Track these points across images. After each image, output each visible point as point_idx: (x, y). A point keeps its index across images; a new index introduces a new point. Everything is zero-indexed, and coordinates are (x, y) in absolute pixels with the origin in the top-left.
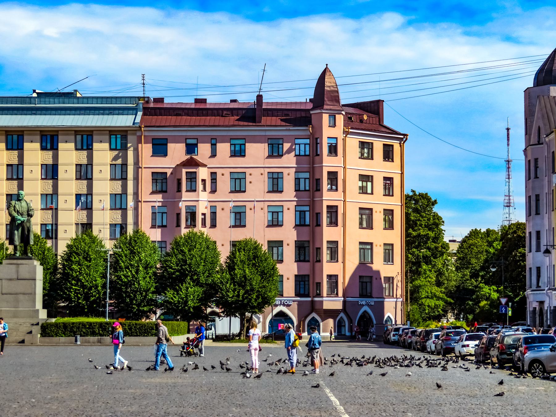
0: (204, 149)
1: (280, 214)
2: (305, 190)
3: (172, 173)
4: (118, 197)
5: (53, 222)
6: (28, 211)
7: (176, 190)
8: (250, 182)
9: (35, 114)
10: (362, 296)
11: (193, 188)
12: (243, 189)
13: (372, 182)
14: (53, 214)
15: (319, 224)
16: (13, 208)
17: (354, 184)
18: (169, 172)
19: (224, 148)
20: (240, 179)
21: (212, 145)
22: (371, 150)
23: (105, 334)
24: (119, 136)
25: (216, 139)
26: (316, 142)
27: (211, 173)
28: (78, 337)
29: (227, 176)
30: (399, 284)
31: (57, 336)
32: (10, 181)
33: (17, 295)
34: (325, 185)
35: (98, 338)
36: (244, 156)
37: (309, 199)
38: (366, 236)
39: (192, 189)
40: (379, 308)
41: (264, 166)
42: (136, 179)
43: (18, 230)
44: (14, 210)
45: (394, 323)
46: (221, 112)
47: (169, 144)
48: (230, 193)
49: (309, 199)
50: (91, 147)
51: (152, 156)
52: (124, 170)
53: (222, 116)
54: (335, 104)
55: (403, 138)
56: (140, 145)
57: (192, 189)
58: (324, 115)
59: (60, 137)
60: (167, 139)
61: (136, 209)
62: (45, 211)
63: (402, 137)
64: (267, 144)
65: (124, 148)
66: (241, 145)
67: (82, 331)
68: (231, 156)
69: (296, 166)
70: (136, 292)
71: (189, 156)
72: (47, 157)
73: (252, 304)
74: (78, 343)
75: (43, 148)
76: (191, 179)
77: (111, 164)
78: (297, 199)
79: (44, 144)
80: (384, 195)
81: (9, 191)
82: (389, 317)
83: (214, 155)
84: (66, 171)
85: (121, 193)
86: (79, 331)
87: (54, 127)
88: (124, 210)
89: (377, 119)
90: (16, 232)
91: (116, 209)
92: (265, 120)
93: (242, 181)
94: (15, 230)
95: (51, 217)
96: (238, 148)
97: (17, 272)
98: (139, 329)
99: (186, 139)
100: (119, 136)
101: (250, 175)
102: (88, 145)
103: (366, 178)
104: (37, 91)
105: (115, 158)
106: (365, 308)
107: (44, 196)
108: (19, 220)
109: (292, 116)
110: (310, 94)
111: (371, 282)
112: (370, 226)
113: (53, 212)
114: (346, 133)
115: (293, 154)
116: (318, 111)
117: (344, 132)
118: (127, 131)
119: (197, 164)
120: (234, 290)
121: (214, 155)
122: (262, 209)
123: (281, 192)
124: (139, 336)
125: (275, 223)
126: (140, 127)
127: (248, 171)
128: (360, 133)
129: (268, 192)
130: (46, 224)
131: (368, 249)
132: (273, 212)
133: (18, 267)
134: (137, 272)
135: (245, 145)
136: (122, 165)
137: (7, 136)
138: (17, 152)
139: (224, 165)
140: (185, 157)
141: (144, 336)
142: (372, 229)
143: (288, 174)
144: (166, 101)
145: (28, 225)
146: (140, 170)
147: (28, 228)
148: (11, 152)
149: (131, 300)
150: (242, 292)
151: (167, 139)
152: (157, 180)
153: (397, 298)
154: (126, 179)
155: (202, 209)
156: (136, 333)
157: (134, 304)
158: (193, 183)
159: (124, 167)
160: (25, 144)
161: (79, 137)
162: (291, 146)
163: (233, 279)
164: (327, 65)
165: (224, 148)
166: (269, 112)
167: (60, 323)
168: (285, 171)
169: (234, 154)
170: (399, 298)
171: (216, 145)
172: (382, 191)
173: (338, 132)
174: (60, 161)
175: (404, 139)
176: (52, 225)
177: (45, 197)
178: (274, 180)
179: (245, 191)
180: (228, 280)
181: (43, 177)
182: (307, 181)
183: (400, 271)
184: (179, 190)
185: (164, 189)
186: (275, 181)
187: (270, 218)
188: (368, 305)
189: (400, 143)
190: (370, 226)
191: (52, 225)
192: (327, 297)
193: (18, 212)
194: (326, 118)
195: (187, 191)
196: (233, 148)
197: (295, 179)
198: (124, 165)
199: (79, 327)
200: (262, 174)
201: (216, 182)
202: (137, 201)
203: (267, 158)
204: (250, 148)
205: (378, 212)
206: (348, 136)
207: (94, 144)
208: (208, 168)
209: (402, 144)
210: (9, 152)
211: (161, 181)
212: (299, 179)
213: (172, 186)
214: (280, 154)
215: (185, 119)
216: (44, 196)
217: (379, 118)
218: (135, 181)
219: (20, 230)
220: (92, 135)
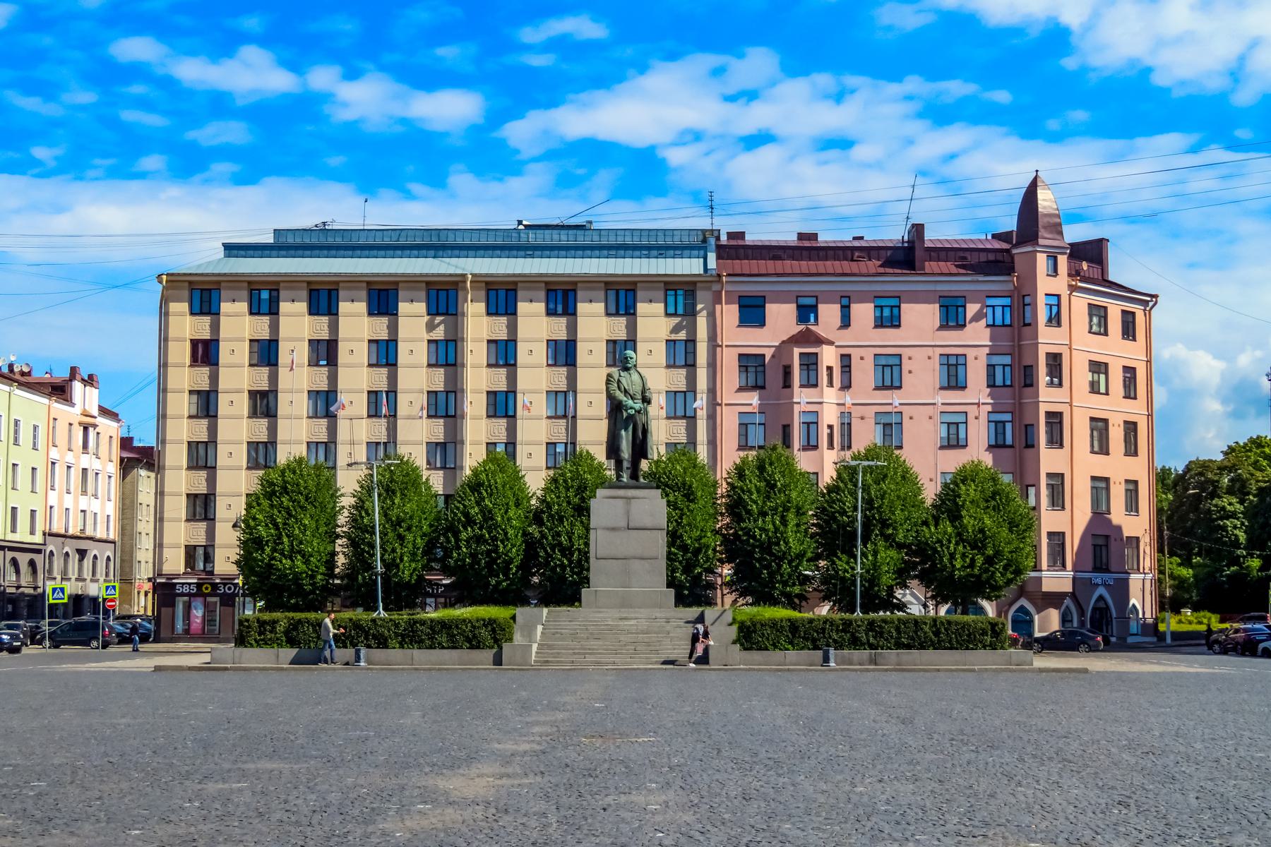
0: (829, 314)
1: (962, 427)
2: (1005, 386)
3: (773, 356)
4: (680, 398)
5: (567, 440)
6: (644, 391)
7: (781, 384)
8: (910, 372)
9: (532, 256)
10: (1097, 569)
11: (813, 381)
12: (896, 384)
13: (1106, 373)
14: (567, 426)
15: (1031, 444)
16: (616, 385)
17: (1080, 375)
18: (768, 353)
19: (863, 312)
20: (891, 366)
21: (842, 307)
22: (1103, 319)
23: (881, 643)
24: (680, 292)
25: (849, 297)
26: (1022, 301)
27: (842, 356)
28: (832, 651)
29: (869, 363)
30: (1148, 551)
31: (775, 646)
32: (493, 369)
33: (628, 561)
34: (1043, 377)
35: (871, 654)
36: (899, 326)
37: (1012, 401)
38: (1101, 465)
39: (811, 383)
40: (1121, 589)
41: (933, 344)
42: (712, 365)
43: (626, 429)
44: (619, 388)
45: (1141, 616)
46: (849, 253)
47: (767, 305)
48: (874, 389)
49: (1012, 401)
50: (632, 311)
51: (739, 326)
52: (690, 349)
53: (852, 260)
54: (1059, 237)
55: (1148, 301)
56: (718, 307)
57: (811, 383)
58: (1038, 254)
59: (580, 294)
60: (764, 297)
61: (712, 417)
62: (554, 420)
63: (1149, 299)
64: (937, 305)
65: (691, 313)
66: (892, 307)
67: (830, 637)
68: (876, 327)
69: (990, 344)
70: (781, 559)
71: (802, 327)
72: (558, 328)
73: (995, 581)
74: (832, 664)
75: (550, 313)
76: (808, 365)
77: (667, 341)
78: (992, 401)
79: (552, 306)
80: (1124, 397)
81: (491, 386)
82: (1134, 605)
83: (846, 322)
84: (591, 351)
85: (685, 390)
86: (825, 637)
87: (570, 275)
88: (691, 420)
89: (1100, 271)
90: (623, 432)
91: (675, 418)
92: (931, 266)
93: (896, 369)
94: (621, 430)
95: (564, 431)
96: (887, 312)
97: (628, 513)
98: (957, 632)
99: (797, 297)
100: (680, 292)
101: (910, 358)
102: (626, 308)
103: (1098, 367)
104: (524, 223)
105: (676, 330)
106: (1101, 591)
107: (553, 394)
108: (631, 408)
109: (973, 259)
110: (1010, 223)
111: (1107, 546)
112: (1104, 450)
113: (567, 423)
114: (1073, 289)
115: (983, 322)
116: (1029, 249)
117: (1070, 286)
118: (695, 283)
119: (819, 341)
120: (964, 556)
121: (846, 322)
122: (930, 418)
123: (964, 388)
124: (957, 649)
125: (953, 442)
126: (719, 276)
127: (906, 353)
128: (1090, 289)
129: (942, 388)
130: (555, 444)
131: (1102, 488)
132: (949, 424)
133: (628, 504)
134: (784, 522)
135: (899, 307)
136: (686, 341)
137: (488, 291)
138: (505, 318)
139: (865, 341)
140: (797, 329)
141: (967, 648)
142: (1107, 454)
143: (976, 358)
144: (748, 237)
145: (644, 419)
146: (719, 349)
147: (644, 425)
148: (494, 318)
149: (771, 575)
150: (980, 560)
151: (764, 297)
152: (747, 367)
153: (1145, 574)
154: (694, 365)
155: (830, 416)
156: (950, 642)
157: (778, 582)
158: (812, 374)
159: (690, 345)
160: (519, 304)
161: (612, 294)
162: (981, 309)
163: (959, 534)
164: (1037, 171)
165: (863, 312)
166: (932, 253)
167: (782, 621)
168: (971, 353)
169: (880, 323)
170: (1148, 573)
171: (849, 307)
172: (1121, 392)
173: (1060, 284)
174: (581, 334)
175: (1151, 304)
176: (566, 444)
177: (553, 396)
178: (951, 367)
179: (900, 387)
180: (950, 536)
181: (550, 362)
182: (1008, 369)
183: (1148, 528)
184: (787, 384)
185: (760, 383)
186: (953, 369)
187: (944, 434)
188: (1105, 585)
189: (1145, 310)
190: (1104, 450)
191: (566, 444)
192: (1048, 570)
193: (626, 392)
194: (1042, 259)
195: (802, 386)
196: (878, 314)
197: (988, 365)
198: (691, 342)
199: (823, 629)
200: (929, 358)
201: (850, 371)
202: (713, 404)
203: (937, 330)
204: (910, 312)
205: (1116, 425)
206: (1074, 294)
207: (639, 305)
208: (837, 347)
209: (1147, 312)
210: (491, 318)
211: (753, 369)
212: (994, 366)
213: (774, 378)
214: (961, 322)
215: (789, 266)
216: (553, 394)
217: (1102, 270)
218: (711, 369)
219: (631, 428)
220: (634, 291)
